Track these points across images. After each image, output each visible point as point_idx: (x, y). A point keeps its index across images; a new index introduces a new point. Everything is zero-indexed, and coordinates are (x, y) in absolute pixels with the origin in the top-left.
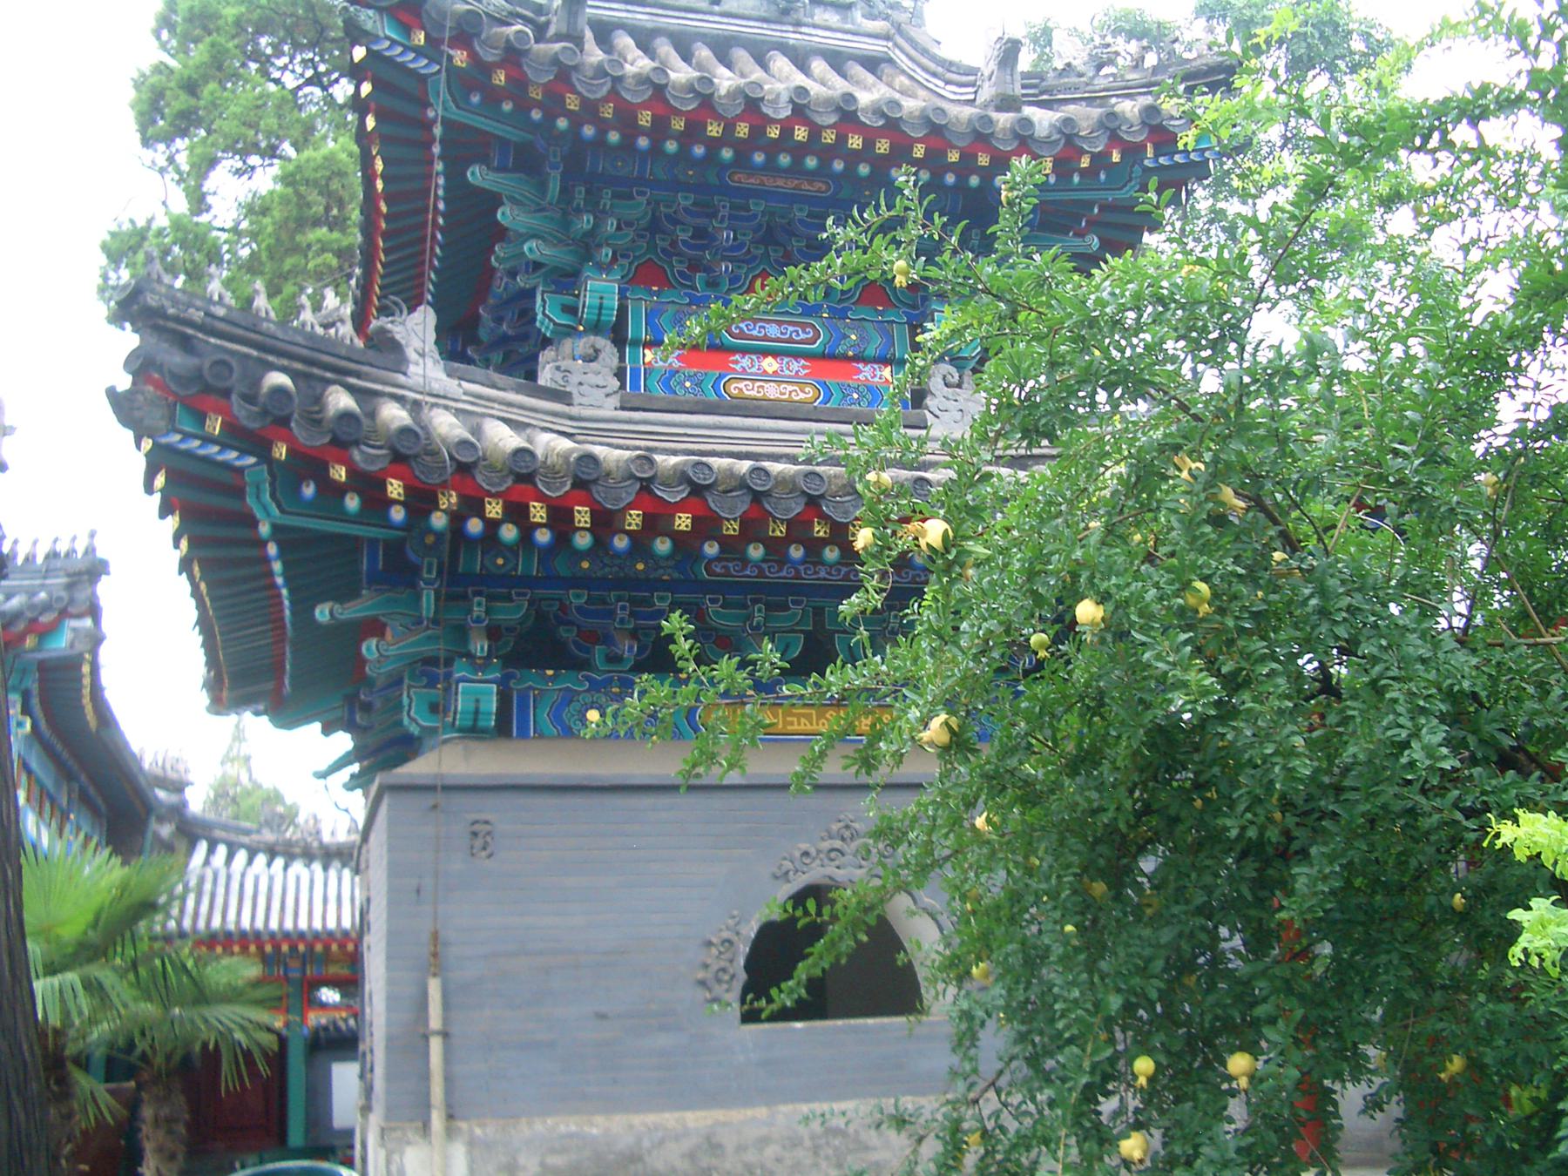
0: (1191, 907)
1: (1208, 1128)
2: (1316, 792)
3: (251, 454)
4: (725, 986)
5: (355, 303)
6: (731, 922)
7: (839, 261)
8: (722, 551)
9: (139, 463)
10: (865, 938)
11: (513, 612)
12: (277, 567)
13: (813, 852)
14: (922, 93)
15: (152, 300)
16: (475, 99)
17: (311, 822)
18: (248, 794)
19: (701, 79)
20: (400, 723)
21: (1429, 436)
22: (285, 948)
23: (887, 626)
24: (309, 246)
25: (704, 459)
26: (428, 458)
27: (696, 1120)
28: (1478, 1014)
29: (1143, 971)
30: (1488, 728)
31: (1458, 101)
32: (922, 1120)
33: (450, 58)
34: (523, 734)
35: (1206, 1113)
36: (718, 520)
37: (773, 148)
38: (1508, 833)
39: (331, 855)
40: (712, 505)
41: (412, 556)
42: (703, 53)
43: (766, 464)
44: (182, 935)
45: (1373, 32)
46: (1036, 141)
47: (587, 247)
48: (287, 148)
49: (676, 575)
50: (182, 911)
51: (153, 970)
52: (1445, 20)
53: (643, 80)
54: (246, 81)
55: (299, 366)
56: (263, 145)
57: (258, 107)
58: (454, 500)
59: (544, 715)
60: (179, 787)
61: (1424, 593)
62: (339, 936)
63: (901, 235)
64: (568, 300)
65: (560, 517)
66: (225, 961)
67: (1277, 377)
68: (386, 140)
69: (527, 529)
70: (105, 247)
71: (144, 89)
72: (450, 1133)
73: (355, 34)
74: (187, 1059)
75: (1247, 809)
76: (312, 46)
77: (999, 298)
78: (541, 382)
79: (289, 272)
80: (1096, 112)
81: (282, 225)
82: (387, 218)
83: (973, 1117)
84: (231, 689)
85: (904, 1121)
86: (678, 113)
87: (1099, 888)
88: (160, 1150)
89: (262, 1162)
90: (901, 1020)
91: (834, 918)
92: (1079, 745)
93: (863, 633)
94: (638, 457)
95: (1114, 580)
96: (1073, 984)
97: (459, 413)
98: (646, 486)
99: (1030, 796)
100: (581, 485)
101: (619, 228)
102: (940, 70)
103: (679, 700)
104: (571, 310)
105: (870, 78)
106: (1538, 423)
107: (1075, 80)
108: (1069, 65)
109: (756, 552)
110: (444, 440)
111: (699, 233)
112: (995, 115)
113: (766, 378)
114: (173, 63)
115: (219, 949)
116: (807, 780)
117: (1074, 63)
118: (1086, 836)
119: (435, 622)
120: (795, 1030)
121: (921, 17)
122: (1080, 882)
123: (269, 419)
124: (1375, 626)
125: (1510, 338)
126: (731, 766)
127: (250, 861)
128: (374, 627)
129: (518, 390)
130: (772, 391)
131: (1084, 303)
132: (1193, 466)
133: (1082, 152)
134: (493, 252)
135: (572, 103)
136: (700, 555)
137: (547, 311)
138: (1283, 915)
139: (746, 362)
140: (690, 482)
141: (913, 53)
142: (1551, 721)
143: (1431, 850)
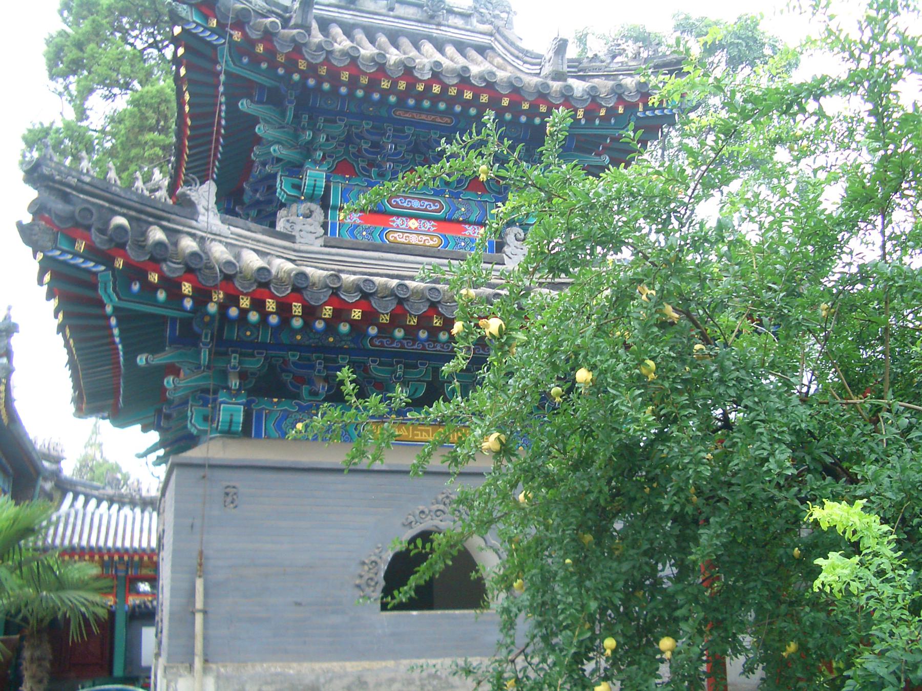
0: (641, 550)
1: (646, 681)
2: (716, 486)
3: (103, 264)
4: (372, 589)
5: (171, 177)
6: (377, 551)
7: (448, 164)
8: (379, 331)
9: (35, 267)
10: (450, 563)
11: (255, 364)
12: (116, 332)
13: (427, 511)
14: (510, 68)
15: (46, 171)
16: (245, 60)
17: (136, 483)
18: (100, 465)
19: (379, 54)
20: (186, 427)
21: (791, 279)
22: (116, 558)
23: (470, 380)
24: (146, 143)
25: (371, 278)
26: (207, 271)
27: (352, 667)
28: (805, 618)
29: (611, 588)
30: (817, 451)
31: (809, 85)
32: (480, 671)
33: (231, 36)
34: (258, 435)
35: (645, 672)
36: (376, 314)
37: (420, 97)
38: (817, 513)
39: (146, 504)
40: (374, 305)
41: (196, 328)
42: (382, 39)
43: (407, 282)
44: (54, 547)
45: (777, 44)
46: (574, 99)
47: (308, 150)
48: (136, 85)
49: (352, 345)
50: (46, 535)
51: (31, 569)
52: (808, 37)
53: (345, 53)
54: (113, 44)
55: (133, 213)
56: (122, 82)
57: (119, 59)
58: (221, 296)
59: (271, 426)
60: (57, 460)
61: (786, 369)
62: (149, 552)
63: (484, 151)
64: (296, 181)
65: (284, 309)
66: (77, 566)
67: (699, 242)
68: (192, 82)
69: (265, 315)
70: (25, 139)
71: (51, 45)
72: (205, 670)
73: (175, 19)
74: (54, 621)
75: (675, 495)
76: (153, 25)
77: (540, 189)
78: (278, 229)
79: (133, 157)
80: (610, 83)
81: (130, 130)
82: (191, 128)
83: (511, 671)
84: (88, 403)
85: (470, 671)
86: (365, 74)
87: (588, 538)
88: (33, 677)
89: (94, 685)
90: (472, 612)
91: (432, 550)
92: (580, 453)
93: (456, 384)
94: (331, 275)
95: (599, 357)
96: (569, 594)
97: (227, 245)
98: (335, 292)
99: (551, 482)
100: (297, 290)
101: (327, 140)
102: (521, 55)
103: (345, 418)
104: (297, 187)
105: (480, 58)
106: (851, 274)
107: (599, 64)
108: (596, 55)
109: (399, 333)
110: (217, 261)
111: (375, 145)
112: (551, 83)
113: (410, 231)
114: (69, 31)
115: (77, 557)
116: (420, 469)
117: (599, 54)
118: (580, 507)
119: (208, 367)
120: (413, 616)
121: (511, 24)
122: (577, 534)
123: (113, 245)
124: (752, 390)
125: (838, 225)
126: (375, 459)
127: (98, 506)
128: (173, 370)
129: (264, 233)
130: (414, 239)
131: (588, 194)
132: (649, 292)
133: (601, 106)
134: (253, 151)
135: (302, 65)
136: (365, 335)
137: (283, 187)
138: (692, 557)
139: (399, 221)
140: (361, 291)
141: (505, 44)
142: (854, 449)
143: (782, 522)
